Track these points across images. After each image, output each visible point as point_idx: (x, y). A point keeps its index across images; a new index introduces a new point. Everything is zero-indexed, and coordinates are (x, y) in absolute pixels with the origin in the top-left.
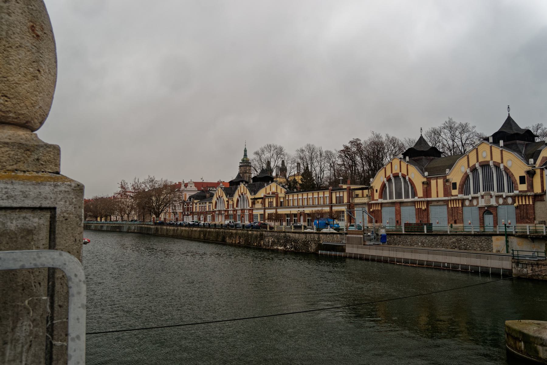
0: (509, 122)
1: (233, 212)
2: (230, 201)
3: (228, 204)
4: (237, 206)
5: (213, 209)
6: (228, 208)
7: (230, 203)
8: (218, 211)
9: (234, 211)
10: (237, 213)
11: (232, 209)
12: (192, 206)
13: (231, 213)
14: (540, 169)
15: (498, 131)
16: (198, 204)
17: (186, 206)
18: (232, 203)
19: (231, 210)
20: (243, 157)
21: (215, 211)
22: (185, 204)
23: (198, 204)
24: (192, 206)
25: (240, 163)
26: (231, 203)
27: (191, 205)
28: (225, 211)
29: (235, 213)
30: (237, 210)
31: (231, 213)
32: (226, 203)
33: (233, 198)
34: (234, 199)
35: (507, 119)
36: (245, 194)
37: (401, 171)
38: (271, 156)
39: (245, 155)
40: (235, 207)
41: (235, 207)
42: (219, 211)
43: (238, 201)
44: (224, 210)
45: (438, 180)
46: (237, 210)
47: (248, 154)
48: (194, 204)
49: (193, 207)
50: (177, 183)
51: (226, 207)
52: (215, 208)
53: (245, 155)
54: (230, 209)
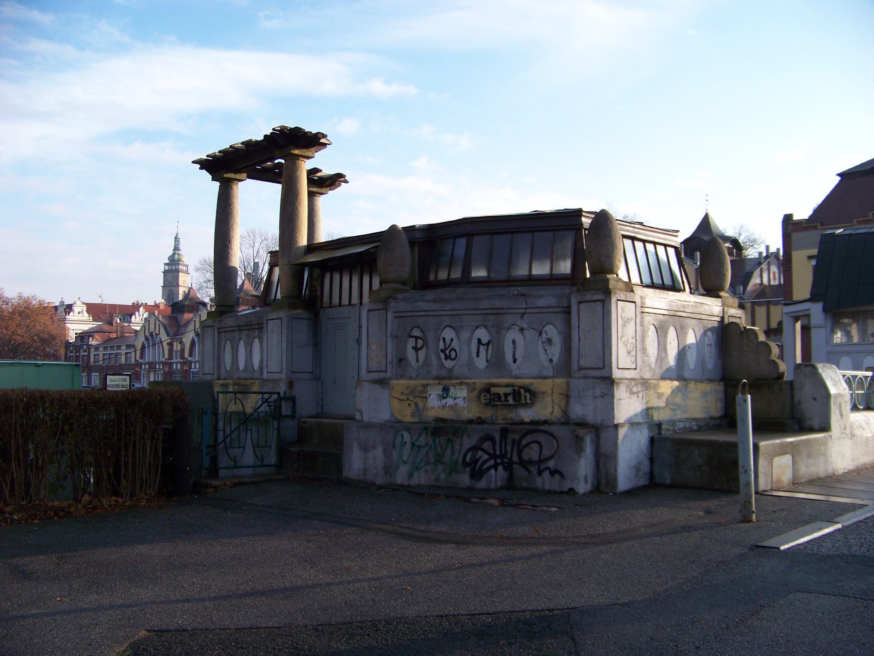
0: (705, 223)
1: (182, 367)
2: (175, 344)
3: (171, 351)
4: (191, 355)
5: (136, 360)
6: (171, 357)
7: (175, 348)
8: (147, 363)
9: (183, 364)
10: (190, 368)
11: (179, 360)
12: (86, 354)
13: (177, 367)
14: (752, 302)
15: (690, 237)
16: (101, 349)
17: (72, 352)
18: (179, 348)
19: (177, 363)
20: (171, 253)
21: (141, 364)
22: (71, 348)
23: (101, 349)
24: (86, 354)
25: (165, 264)
26: (177, 347)
27: (85, 351)
28: (164, 364)
29: (186, 368)
30: (191, 363)
31: (177, 367)
32: (166, 348)
33: (181, 338)
34: (184, 340)
35: (704, 217)
36: (157, 335)
37: (155, 331)
38: (255, 253)
39: (176, 248)
40: (186, 355)
41: (186, 355)
42: (150, 363)
43: (193, 343)
44: (160, 363)
45: (772, 308)
46: (191, 363)
47: (181, 247)
48: (93, 350)
49: (89, 356)
50: (306, 131)
51: (166, 356)
52: (142, 357)
53: (176, 248)
54: (175, 360)
